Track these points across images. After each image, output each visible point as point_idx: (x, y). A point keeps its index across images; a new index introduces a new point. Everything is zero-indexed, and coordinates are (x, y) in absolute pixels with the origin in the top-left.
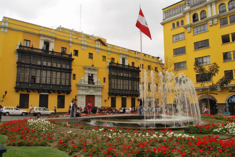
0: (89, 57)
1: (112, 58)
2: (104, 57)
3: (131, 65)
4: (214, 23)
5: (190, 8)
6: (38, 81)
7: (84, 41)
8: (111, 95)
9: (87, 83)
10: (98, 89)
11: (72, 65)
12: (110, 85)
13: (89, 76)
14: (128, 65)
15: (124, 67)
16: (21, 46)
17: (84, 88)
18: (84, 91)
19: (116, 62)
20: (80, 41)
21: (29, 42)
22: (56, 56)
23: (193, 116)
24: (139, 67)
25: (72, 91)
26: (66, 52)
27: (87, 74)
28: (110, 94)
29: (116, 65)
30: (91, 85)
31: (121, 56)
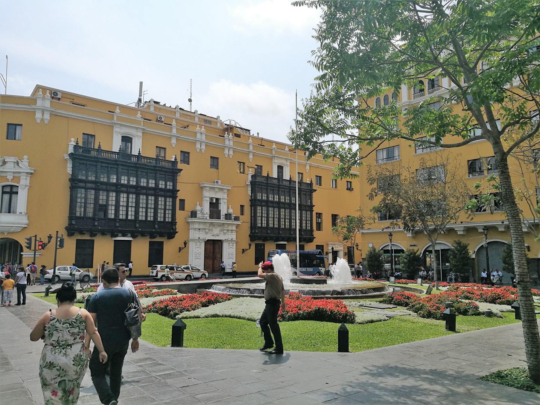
6: (111, 214)
7: (201, 133)
9: (208, 216)
10: (230, 228)
11: (178, 181)
12: (254, 217)
16: (76, 147)
17: (201, 226)
18: (201, 232)
21: (163, 150)
24: (311, 182)
27: (208, 199)
28: (252, 237)
31: (276, 161)
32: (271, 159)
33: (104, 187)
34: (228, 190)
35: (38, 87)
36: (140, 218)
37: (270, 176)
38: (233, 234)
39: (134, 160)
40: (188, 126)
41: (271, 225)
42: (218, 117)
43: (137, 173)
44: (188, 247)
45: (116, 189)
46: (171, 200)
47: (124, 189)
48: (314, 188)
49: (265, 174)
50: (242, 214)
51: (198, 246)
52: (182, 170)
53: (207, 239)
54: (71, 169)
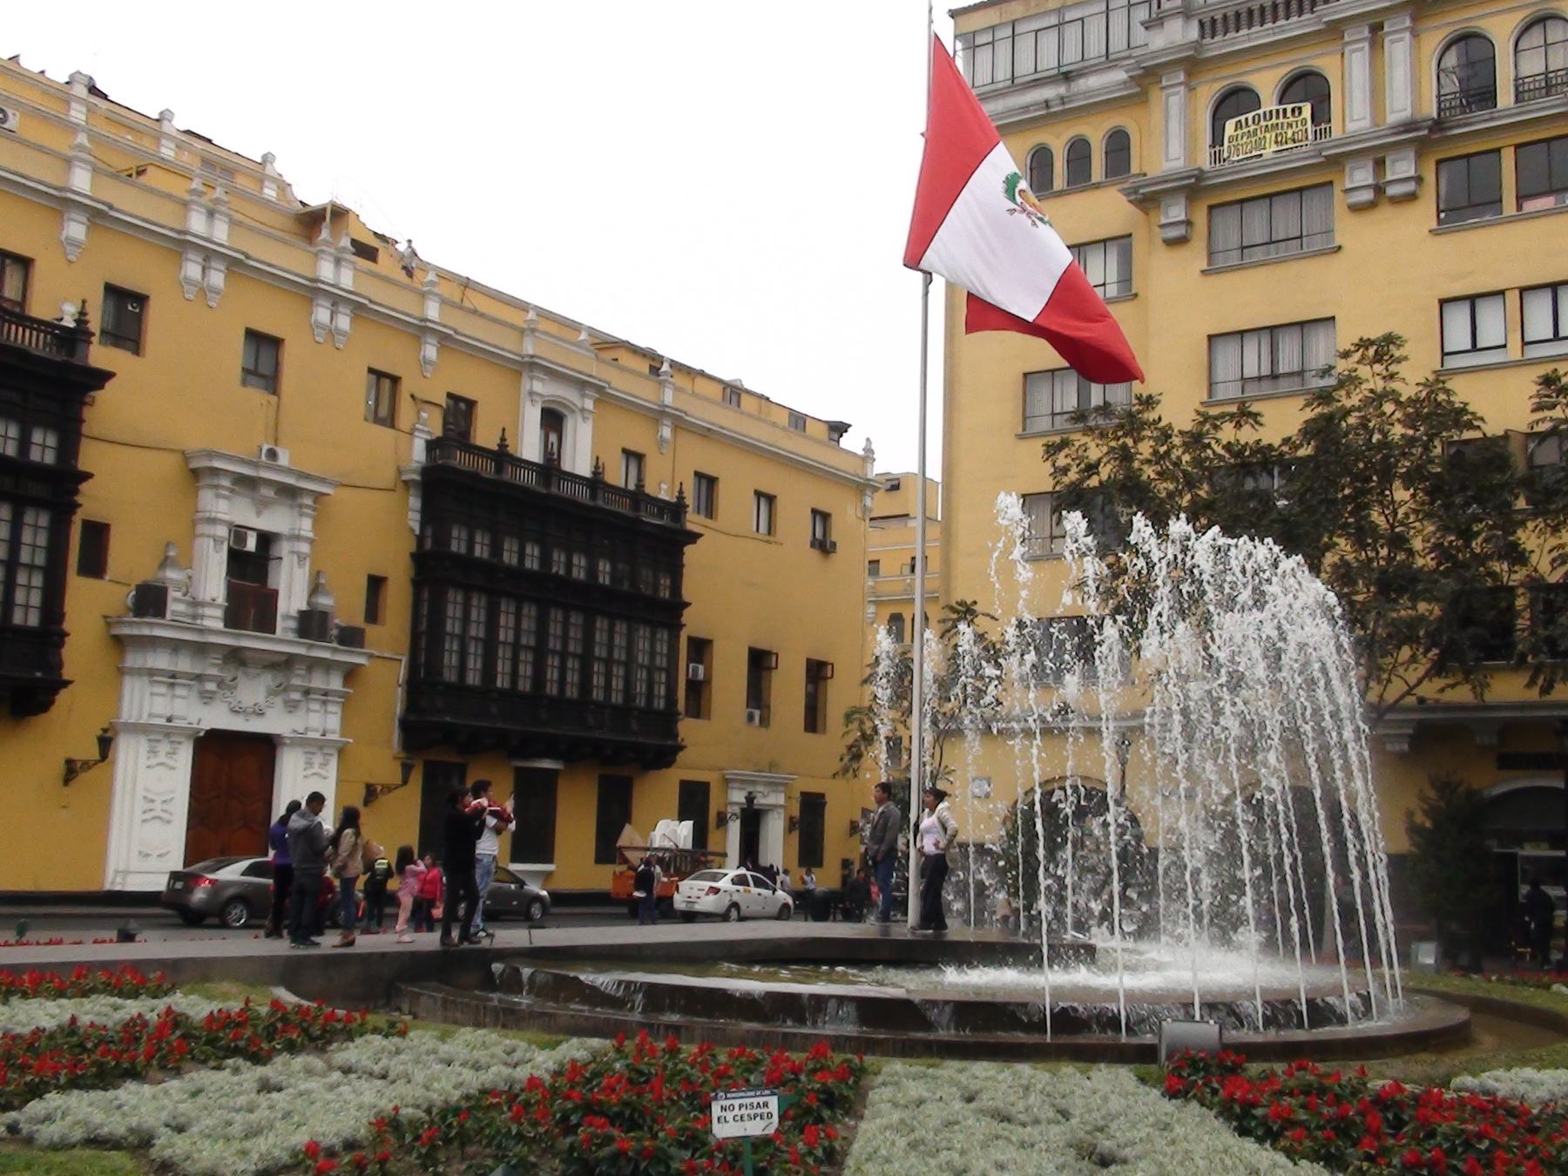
0: (246, 371)
1: (450, 396)
2: (384, 380)
3: (616, 475)
4: (1392, 191)
5: (1194, 33)
7: (211, 214)
9: (214, 619)
10: (318, 681)
11: (85, 429)
14: (496, 448)
17: (184, 664)
18: (180, 691)
19: (485, 435)
20: (170, 207)
23: (1355, 959)
24: (681, 497)
25: (66, 684)
27: (222, 531)
29: (487, 469)
30: (252, 641)
31: (538, 387)
38: (331, 708)
41: (597, 695)
42: (267, 159)
44: (113, 763)
48: (690, 526)
49: (485, 435)
50: (372, 614)
53: (207, 725)
54: (417, 516)
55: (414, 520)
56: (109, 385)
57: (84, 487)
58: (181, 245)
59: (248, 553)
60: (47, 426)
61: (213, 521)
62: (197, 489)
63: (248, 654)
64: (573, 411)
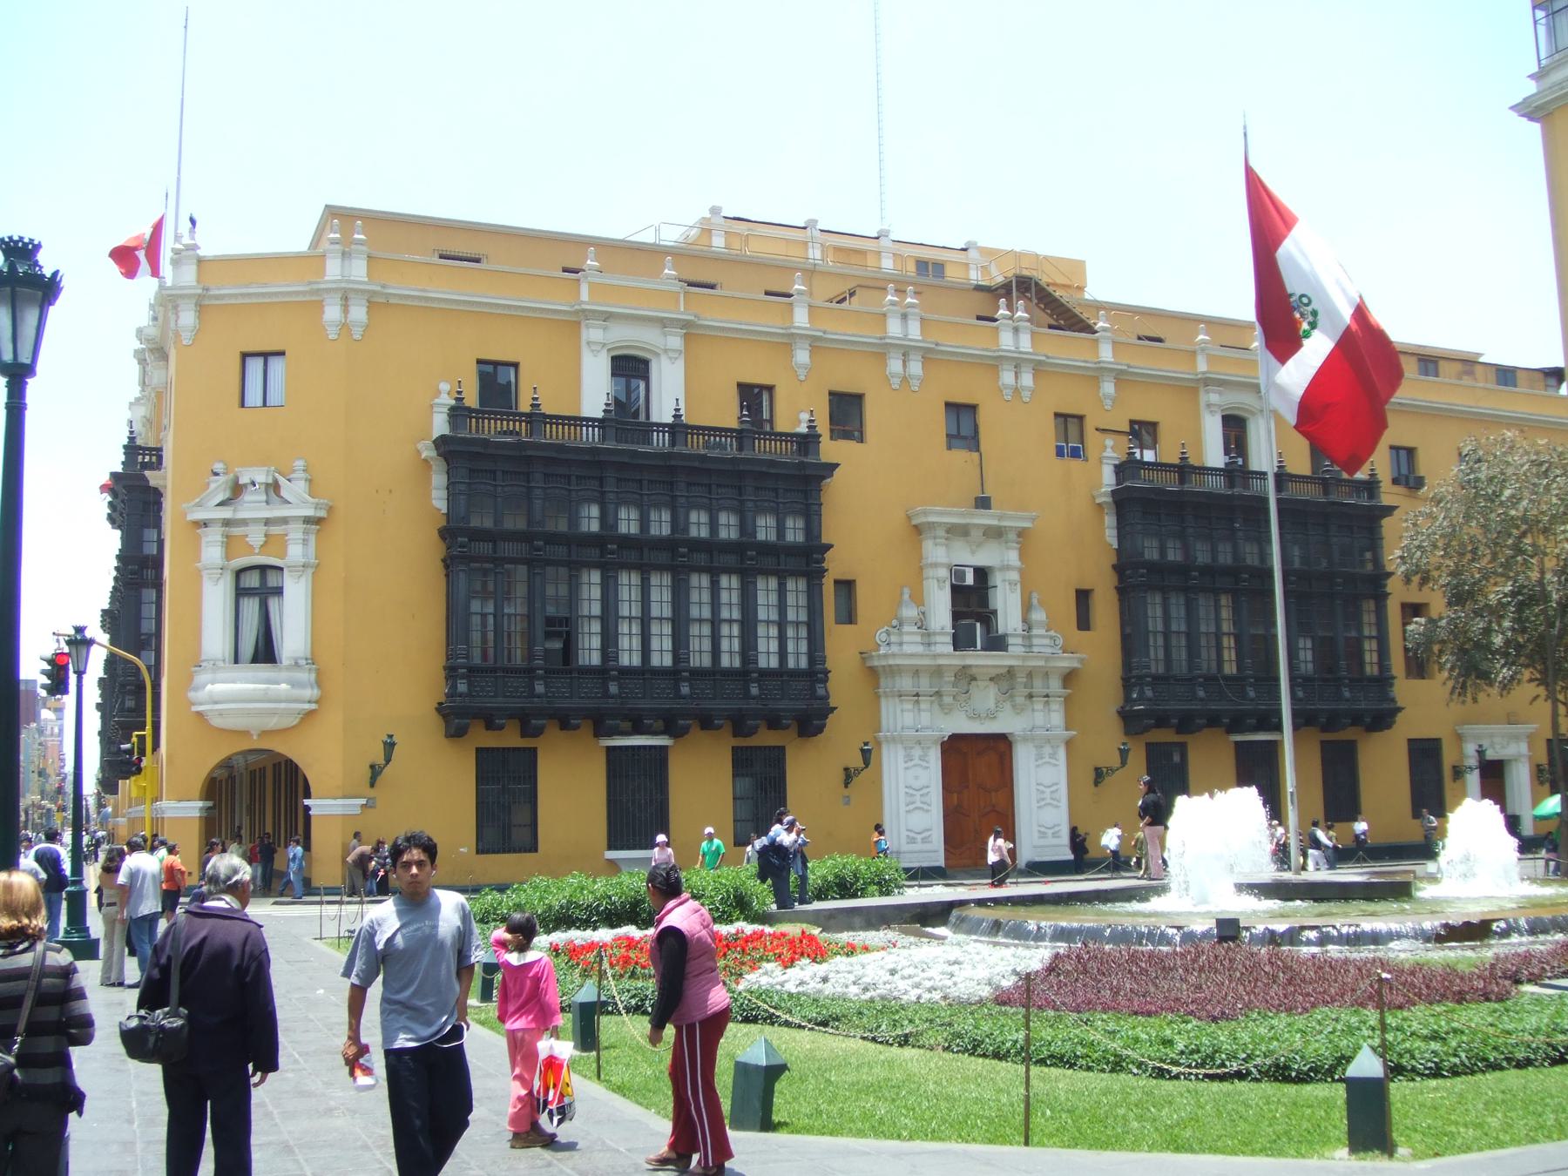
1: (1132, 422)
6: (590, 651)
7: (904, 317)
8: (1146, 729)
9: (944, 646)
12: (1131, 643)
13: (956, 590)
15: (1237, 490)
22: (704, 458)
26: (771, 421)
27: (943, 573)
28: (1130, 721)
31: (1214, 398)
32: (572, 323)
33: (560, 552)
34: (1022, 533)
35: (333, 213)
36: (762, 663)
37: (1193, 461)
39: (660, 441)
40: (852, 295)
43: (601, 486)
45: (602, 556)
46: (802, 584)
47: (701, 558)
51: (1047, 759)
52: (838, 465)
53: (947, 734)
54: (444, 494)
55: (439, 501)
56: (837, 472)
57: (828, 555)
58: (881, 351)
59: (969, 587)
60: (795, 513)
61: (935, 565)
62: (920, 542)
63: (974, 671)
64: (1253, 413)
